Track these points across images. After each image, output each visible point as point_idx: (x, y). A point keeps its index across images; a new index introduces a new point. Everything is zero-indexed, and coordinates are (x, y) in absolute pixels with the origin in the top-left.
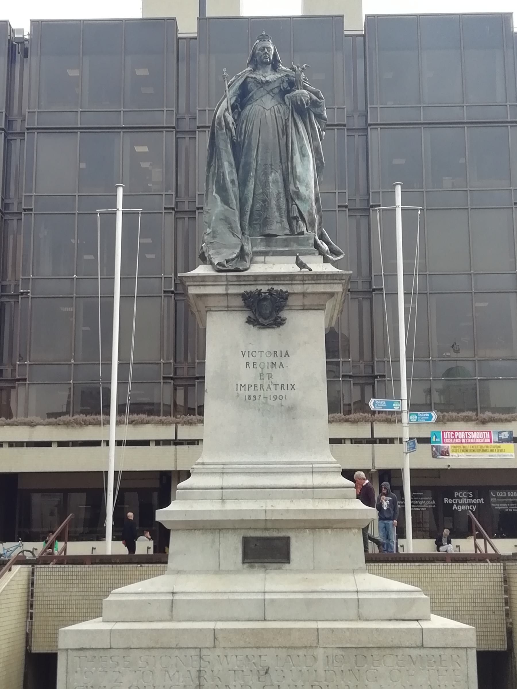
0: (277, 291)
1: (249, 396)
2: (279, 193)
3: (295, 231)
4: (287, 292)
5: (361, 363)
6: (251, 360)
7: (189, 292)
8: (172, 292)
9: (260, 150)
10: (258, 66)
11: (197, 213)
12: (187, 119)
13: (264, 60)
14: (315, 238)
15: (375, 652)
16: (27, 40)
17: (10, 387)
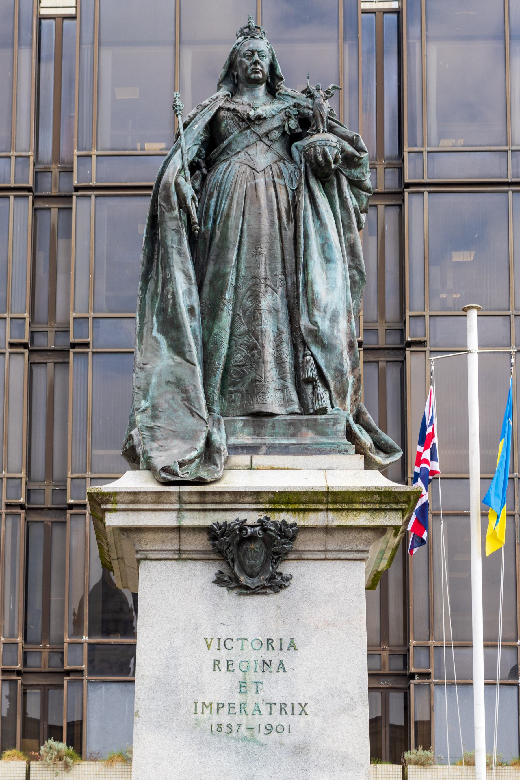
0: (275, 523)
1: (220, 725)
3: (311, 406)
4: (295, 524)
5: (384, 650)
6: (223, 655)
8: (22, 506)
9: (244, 249)
10: (241, 85)
11: (71, 354)
12: (55, 171)
13: (253, 76)
14: (348, 421)
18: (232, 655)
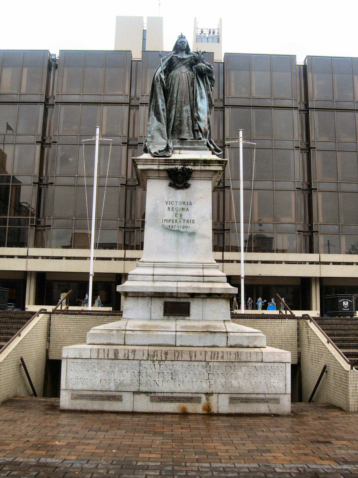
2: (188, 117)
6: (171, 206)
7: (138, 168)
15: (236, 364)
16: (57, 60)
17: (43, 230)
18: (174, 206)
